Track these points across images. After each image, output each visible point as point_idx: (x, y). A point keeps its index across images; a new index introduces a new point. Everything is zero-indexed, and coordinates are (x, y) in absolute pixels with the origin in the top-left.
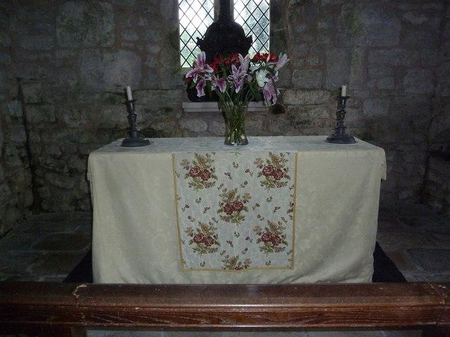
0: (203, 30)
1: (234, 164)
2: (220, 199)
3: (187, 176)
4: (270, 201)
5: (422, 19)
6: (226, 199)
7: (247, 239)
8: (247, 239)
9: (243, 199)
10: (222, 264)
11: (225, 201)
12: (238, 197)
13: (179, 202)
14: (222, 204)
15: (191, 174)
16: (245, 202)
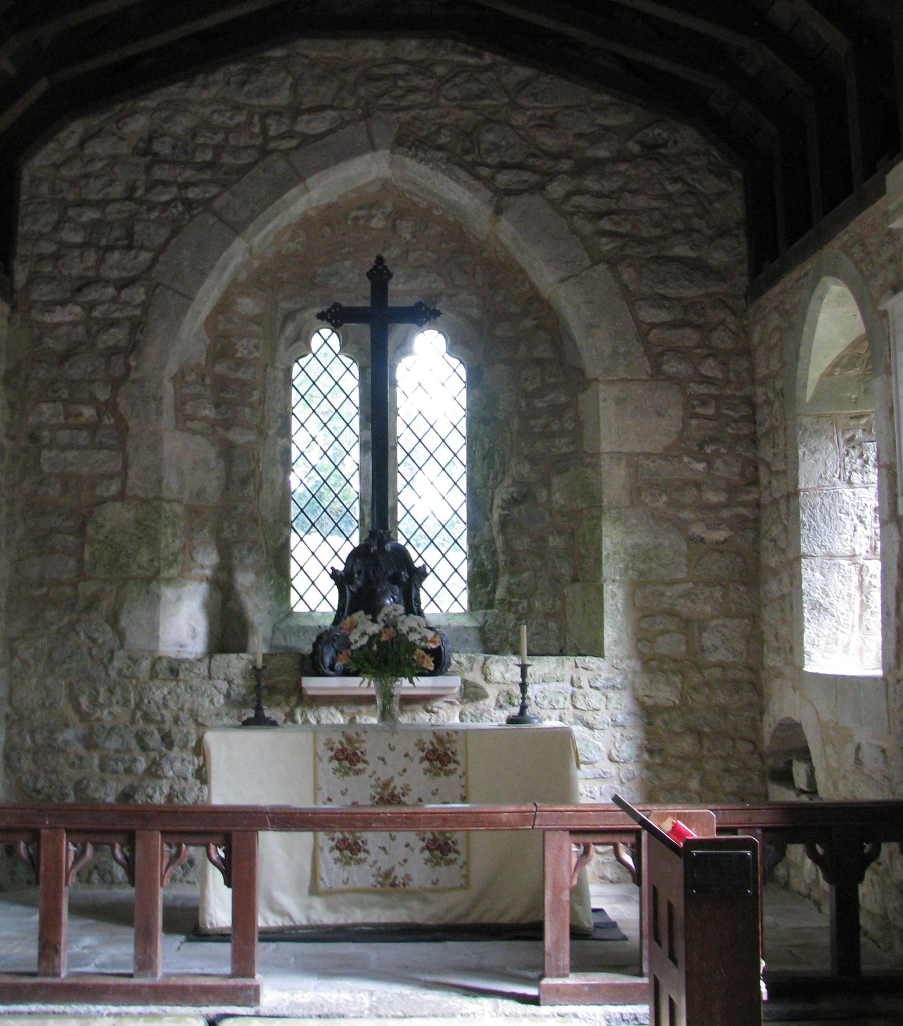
0: (806, 574)
1: (389, 745)
2: (372, 791)
3: (331, 759)
4: (436, 794)
5: (720, 535)
6: (379, 790)
7: (406, 755)
8: (406, 755)
9: (401, 791)
10: (372, 880)
11: (378, 793)
12: (395, 788)
13: (320, 793)
14: (374, 797)
15: (336, 757)
16: (403, 795)
